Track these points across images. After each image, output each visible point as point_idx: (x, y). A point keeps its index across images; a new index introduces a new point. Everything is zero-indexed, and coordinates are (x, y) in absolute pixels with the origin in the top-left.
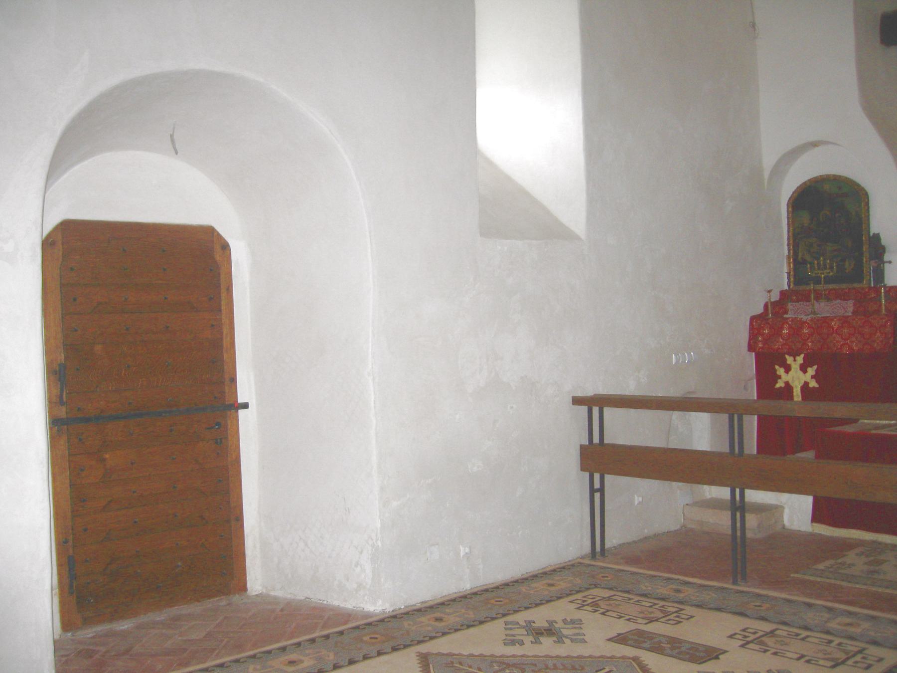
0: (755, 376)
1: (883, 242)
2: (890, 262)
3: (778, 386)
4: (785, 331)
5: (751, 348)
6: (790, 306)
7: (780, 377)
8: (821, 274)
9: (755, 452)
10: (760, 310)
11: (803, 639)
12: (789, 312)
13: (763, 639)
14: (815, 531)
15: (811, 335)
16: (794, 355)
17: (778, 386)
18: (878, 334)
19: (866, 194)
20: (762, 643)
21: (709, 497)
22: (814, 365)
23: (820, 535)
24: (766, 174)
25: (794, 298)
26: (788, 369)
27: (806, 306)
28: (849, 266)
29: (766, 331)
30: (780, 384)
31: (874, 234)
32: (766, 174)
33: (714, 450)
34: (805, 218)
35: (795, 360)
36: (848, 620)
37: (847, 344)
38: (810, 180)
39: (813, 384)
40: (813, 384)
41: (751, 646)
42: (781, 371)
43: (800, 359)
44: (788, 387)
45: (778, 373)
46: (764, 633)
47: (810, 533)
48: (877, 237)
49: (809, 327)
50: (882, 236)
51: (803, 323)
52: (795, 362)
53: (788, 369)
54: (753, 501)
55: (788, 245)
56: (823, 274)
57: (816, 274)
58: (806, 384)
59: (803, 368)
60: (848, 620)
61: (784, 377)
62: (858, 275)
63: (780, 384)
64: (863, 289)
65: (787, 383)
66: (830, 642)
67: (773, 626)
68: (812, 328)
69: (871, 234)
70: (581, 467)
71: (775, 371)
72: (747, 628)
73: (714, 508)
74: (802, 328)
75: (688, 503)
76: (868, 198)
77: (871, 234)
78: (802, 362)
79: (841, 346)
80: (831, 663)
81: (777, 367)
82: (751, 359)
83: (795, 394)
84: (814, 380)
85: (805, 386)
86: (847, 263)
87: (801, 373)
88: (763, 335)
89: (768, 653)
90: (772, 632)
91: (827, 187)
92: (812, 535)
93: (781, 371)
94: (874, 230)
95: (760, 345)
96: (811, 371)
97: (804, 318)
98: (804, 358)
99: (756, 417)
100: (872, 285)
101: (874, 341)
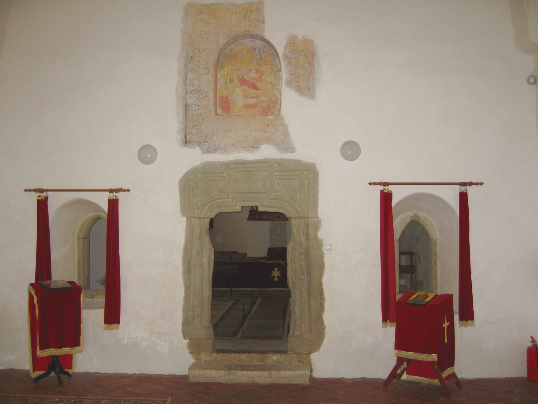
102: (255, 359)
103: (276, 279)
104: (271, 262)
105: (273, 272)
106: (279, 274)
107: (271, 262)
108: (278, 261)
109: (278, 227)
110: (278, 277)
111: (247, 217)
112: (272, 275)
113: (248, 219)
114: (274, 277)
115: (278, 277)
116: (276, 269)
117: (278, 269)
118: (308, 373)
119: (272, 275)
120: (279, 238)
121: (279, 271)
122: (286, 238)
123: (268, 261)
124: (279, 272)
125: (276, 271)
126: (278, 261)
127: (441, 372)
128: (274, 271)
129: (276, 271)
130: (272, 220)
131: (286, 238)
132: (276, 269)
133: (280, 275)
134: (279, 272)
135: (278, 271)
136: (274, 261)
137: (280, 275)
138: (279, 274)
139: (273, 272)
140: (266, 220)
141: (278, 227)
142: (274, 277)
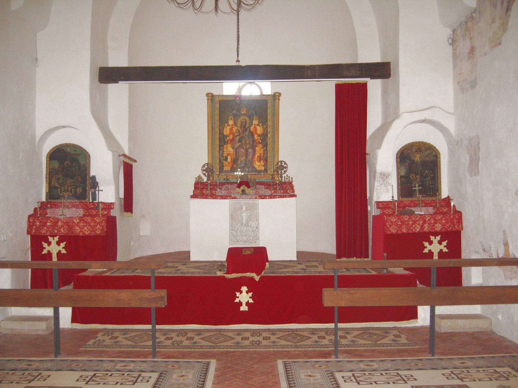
0: (30, 249)
1: (97, 180)
2: (102, 191)
3: (43, 253)
4: (48, 224)
5: (28, 233)
6: (49, 211)
7: (45, 248)
8: (66, 194)
9: (30, 288)
10: (32, 212)
11: (111, 375)
12: (49, 214)
13: (93, 379)
14: (73, 327)
15: (62, 226)
16: (53, 236)
17: (43, 253)
18: (98, 226)
19: (89, 156)
20: (93, 381)
21: (10, 315)
22: (42, 243)
23: (76, 329)
24: (37, 140)
25: (49, 206)
26: (49, 244)
27: (58, 210)
28: (79, 190)
29: (38, 224)
30: (45, 252)
31: (92, 176)
32: (37, 140)
33: (14, 288)
34: (56, 164)
35: (435, 238)
36: (124, 364)
37: (82, 231)
38: (60, 145)
39: (64, 251)
40: (64, 251)
41: (90, 383)
42: (45, 245)
43: (57, 239)
44: (50, 254)
45: (44, 246)
46: (91, 377)
47: (71, 328)
48: (94, 177)
49: (51, 221)
50: (96, 177)
51: (58, 220)
52: (435, 240)
53: (49, 244)
54: (37, 315)
55: (46, 178)
56: (67, 194)
57: (62, 194)
58: (60, 251)
59: (58, 243)
60: (124, 364)
61: (47, 248)
62: (83, 196)
63: (45, 252)
64: (87, 203)
65: (49, 251)
66: (124, 374)
67: (92, 373)
68: (53, 222)
69: (91, 176)
70: (441, 268)
71: (42, 245)
72: (44, 380)
73: (19, 321)
74: (58, 223)
75: (2, 319)
76: (90, 158)
77: (91, 176)
78: (57, 240)
79: (79, 232)
80: (132, 383)
81: (43, 243)
82: (28, 239)
83: (53, 257)
84: (64, 250)
85: (59, 254)
86: (78, 189)
87: (57, 246)
88: (36, 225)
89: (101, 384)
90: (95, 375)
91: (69, 150)
92: (71, 330)
93: (45, 245)
94: (92, 174)
95: (34, 231)
96: (63, 245)
97: (60, 217)
98: (59, 238)
99: (30, 270)
100: (91, 201)
101: (96, 230)
102: (18, 327)
103: (244, 308)
104: (234, 275)
105: (238, 294)
106: (250, 298)
107: (234, 275)
108: (248, 274)
109: (244, 208)
110: (247, 304)
111: (192, 194)
112: (237, 300)
113: (193, 197)
114: (240, 304)
115: (247, 304)
116: (244, 289)
117: (247, 289)
118: (47, 311)
119: (237, 300)
120: (245, 228)
121: (250, 292)
122: (257, 228)
123: (228, 273)
124: (250, 294)
125: (244, 293)
126: (248, 274)
127: (150, 276)
128: (241, 292)
129: (244, 293)
130: (232, 198)
131: (257, 228)
132: (244, 289)
133: (251, 301)
134: (250, 294)
135: (247, 292)
136: (240, 275)
137: (251, 301)
138: (250, 298)
139: (238, 294)
140: (223, 197)
141: (244, 208)
142: (240, 304)
